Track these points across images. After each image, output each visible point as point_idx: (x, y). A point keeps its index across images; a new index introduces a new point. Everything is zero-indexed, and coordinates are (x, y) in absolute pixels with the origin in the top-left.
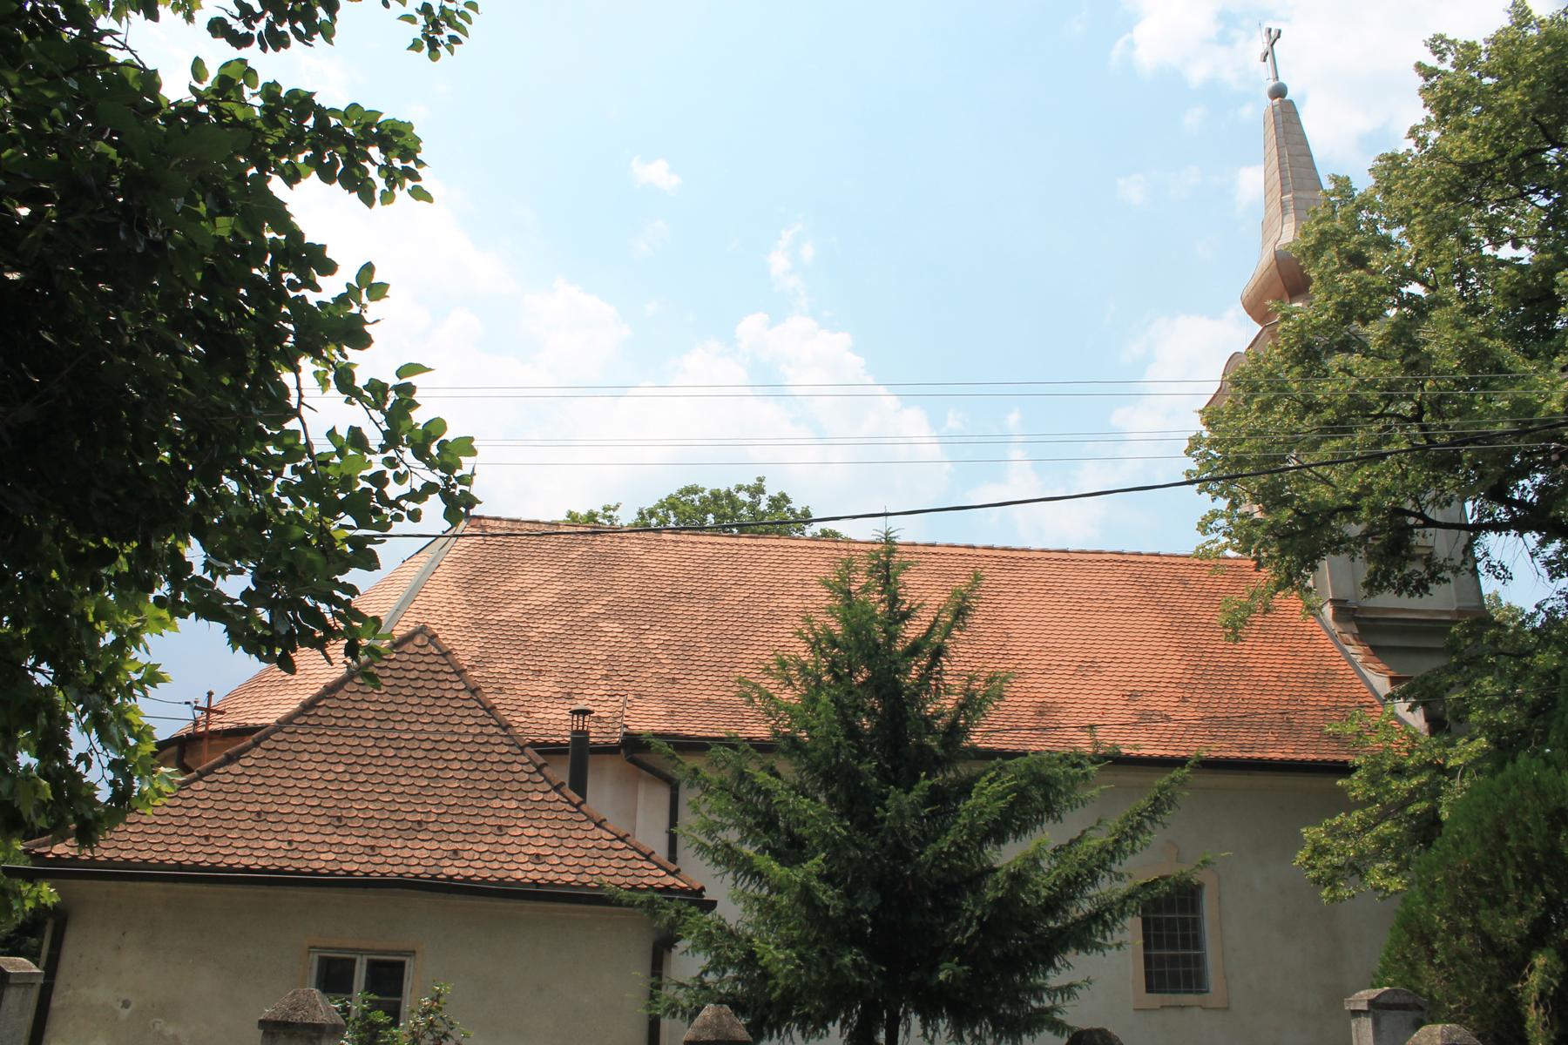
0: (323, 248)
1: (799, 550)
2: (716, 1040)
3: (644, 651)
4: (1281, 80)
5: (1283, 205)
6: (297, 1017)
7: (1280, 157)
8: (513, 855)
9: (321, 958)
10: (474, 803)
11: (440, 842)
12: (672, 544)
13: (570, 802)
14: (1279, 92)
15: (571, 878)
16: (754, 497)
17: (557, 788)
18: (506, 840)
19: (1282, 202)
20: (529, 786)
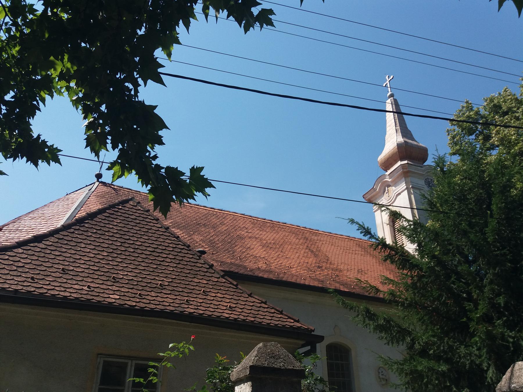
0: (163, 125)
9: (105, 362)
10: (185, 279)
19: (396, 129)
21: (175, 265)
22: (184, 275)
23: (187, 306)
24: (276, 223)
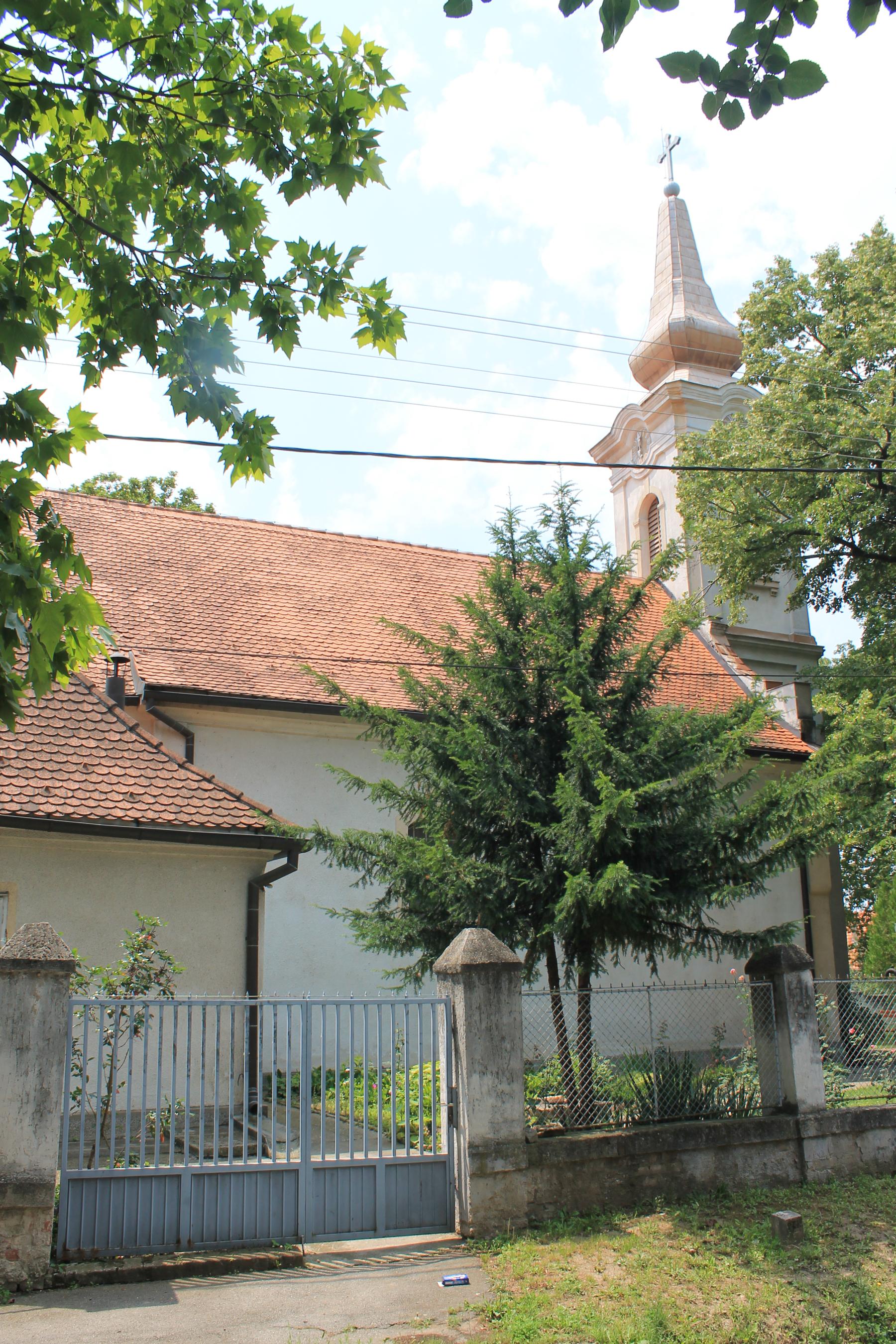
1: (259, 532)
2: (490, 963)
3: (137, 611)
4: (676, 181)
5: (674, 286)
6: (39, 954)
7: (673, 245)
8: (106, 793)
10: (52, 741)
11: (27, 779)
12: (140, 515)
13: (148, 743)
14: (672, 191)
15: (172, 817)
16: (165, 490)
17: (132, 729)
18: (94, 778)
20: (103, 726)
21: (37, 712)
22: (53, 732)
23: (44, 800)
24: (350, 540)
